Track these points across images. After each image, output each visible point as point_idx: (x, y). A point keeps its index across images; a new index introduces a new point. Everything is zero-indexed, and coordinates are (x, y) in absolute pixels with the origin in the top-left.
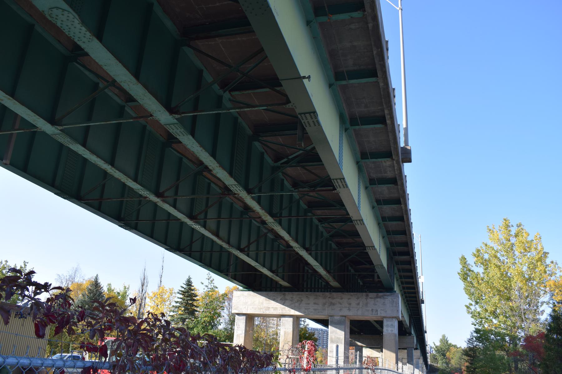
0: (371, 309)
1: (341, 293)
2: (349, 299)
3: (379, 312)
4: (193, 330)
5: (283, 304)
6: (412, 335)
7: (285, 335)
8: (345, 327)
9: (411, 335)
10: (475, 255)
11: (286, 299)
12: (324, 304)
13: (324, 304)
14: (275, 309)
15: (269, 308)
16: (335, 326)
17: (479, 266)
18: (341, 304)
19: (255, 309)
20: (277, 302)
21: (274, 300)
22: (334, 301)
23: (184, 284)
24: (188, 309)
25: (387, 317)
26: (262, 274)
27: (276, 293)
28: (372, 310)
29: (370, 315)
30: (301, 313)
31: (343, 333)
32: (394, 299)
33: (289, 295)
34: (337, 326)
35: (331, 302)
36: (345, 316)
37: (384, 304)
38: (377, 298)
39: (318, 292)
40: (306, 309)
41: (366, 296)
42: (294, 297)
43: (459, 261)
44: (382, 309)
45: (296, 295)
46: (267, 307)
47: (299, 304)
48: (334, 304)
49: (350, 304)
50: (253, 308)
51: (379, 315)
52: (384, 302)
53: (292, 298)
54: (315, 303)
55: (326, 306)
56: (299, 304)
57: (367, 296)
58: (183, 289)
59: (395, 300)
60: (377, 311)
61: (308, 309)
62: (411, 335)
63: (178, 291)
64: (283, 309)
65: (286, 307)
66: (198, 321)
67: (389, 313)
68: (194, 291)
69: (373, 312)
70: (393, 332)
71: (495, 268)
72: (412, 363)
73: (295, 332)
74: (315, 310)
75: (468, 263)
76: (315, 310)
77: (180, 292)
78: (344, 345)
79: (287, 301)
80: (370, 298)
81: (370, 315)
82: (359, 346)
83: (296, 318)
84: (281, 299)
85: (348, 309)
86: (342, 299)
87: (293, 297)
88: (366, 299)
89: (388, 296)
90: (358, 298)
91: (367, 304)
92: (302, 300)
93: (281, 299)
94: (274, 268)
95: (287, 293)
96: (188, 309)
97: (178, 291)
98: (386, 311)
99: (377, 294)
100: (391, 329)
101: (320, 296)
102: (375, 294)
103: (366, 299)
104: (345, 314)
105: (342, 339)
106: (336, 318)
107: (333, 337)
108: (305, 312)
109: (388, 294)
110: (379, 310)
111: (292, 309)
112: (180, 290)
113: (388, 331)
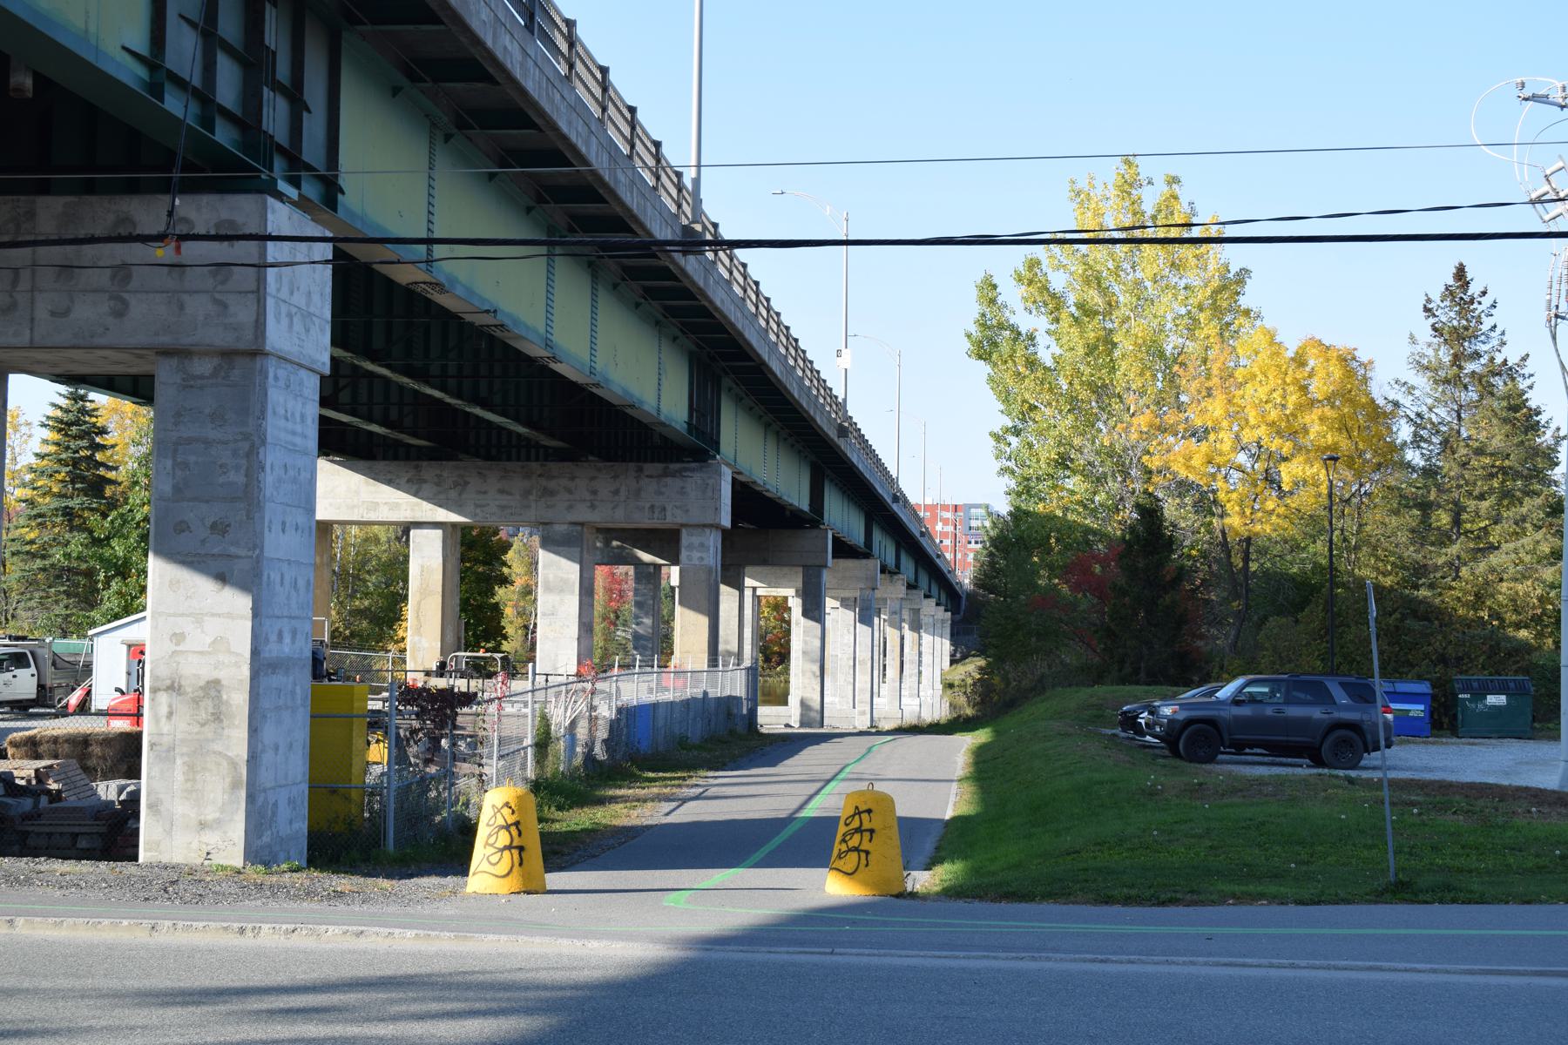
0: (648, 505)
1: (570, 463)
2: (593, 478)
3: (669, 514)
4: (109, 545)
5: (415, 495)
6: (822, 527)
7: (422, 575)
8: (582, 552)
9: (817, 527)
10: (1020, 279)
11: (425, 481)
12: (526, 493)
13: (526, 493)
14: (396, 506)
15: (377, 504)
16: (556, 548)
17: (1034, 312)
18: (570, 492)
19: (339, 508)
20: (399, 489)
21: (389, 483)
22: (552, 484)
23: (60, 395)
24: (83, 479)
25: (691, 526)
26: (371, 433)
27: (396, 462)
28: (652, 507)
29: (647, 521)
30: (460, 513)
31: (577, 567)
32: (709, 478)
33: (430, 470)
34: (561, 549)
35: (545, 489)
36: (582, 524)
37: (682, 492)
38: (667, 476)
39: (509, 459)
40: (477, 506)
41: (637, 471)
42: (445, 474)
43: (974, 293)
44: (677, 504)
45: (448, 471)
46: (372, 502)
47: (460, 495)
48: (552, 493)
49: (594, 492)
50: (331, 505)
51: (669, 519)
52: (683, 488)
53: (439, 476)
54: (501, 491)
55: (531, 497)
56: (460, 495)
57: (640, 470)
58: (59, 413)
59: (711, 482)
60: (664, 509)
61: (484, 506)
62: (817, 527)
63: (44, 419)
64: (416, 508)
65: (425, 503)
66: (123, 515)
67: (696, 516)
68: (97, 417)
69: (653, 512)
70: (705, 562)
71: (1070, 326)
72: (817, 616)
73: (449, 566)
74: (503, 508)
75: (1000, 300)
76: (503, 508)
77: (51, 423)
78: (578, 597)
79: (425, 486)
80: (647, 476)
81: (647, 521)
82: (648, 565)
83: (450, 529)
84: (408, 481)
85: (589, 504)
86: (573, 478)
87: (441, 476)
88: (638, 478)
89: (693, 470)
90: (615, 477)
91: (638, 493)
92: (467, 483)
93: (408, 481)
94: (394, 414)
95: (425, 464)
96: (83, 479)
97: (44, 419)
98: (687, 511)
99: (664, 465)
100: (699, 555)
101: (514, 472)
102: (659, 466)
103: (638, 478)
104: (580, 519)
105: (574, 583)
106: (557, 528)
107: (551, 577)
108: (476, 515)
109: (693, 465)
110: (669, 508)
111: (440, 506)
112: (51, 415)
113: (691, 560)
